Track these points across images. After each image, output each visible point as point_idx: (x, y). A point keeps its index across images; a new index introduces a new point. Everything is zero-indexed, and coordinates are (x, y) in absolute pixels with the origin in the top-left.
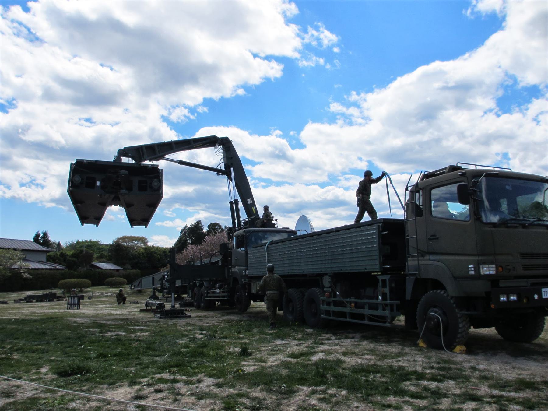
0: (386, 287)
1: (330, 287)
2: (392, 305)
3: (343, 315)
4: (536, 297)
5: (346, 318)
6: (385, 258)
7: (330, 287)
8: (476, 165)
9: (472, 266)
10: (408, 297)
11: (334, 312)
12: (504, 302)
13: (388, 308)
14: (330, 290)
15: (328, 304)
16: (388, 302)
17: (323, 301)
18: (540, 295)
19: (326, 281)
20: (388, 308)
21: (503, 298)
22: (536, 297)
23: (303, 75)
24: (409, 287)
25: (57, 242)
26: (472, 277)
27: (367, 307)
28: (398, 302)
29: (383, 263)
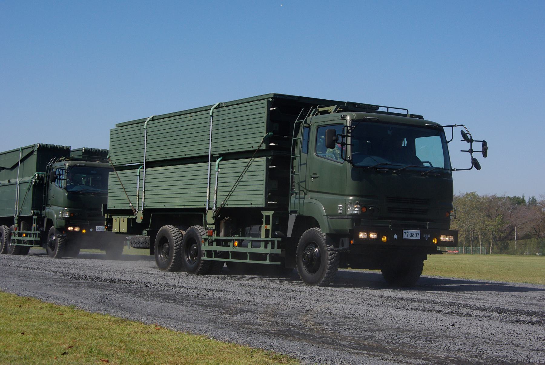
1: (213, 224)
2: (273, 242)
4: (396, 237)
5: (229, 258)
6: (270, 193)
7: (213, 224)
8: (388, 107)
9: (341, 205)
10: (289, 234)
12: (362, 239)
13: (269, 245)
14: (214, 227)
15: (211, 243)
17: (206, 240)
18: (400, 235)
19: (210, 217)
20: (269, 245)
22: (396, 237)
24: (292, 219)
27: (250, 245)
28: (280, 239)
29: (268, 199)
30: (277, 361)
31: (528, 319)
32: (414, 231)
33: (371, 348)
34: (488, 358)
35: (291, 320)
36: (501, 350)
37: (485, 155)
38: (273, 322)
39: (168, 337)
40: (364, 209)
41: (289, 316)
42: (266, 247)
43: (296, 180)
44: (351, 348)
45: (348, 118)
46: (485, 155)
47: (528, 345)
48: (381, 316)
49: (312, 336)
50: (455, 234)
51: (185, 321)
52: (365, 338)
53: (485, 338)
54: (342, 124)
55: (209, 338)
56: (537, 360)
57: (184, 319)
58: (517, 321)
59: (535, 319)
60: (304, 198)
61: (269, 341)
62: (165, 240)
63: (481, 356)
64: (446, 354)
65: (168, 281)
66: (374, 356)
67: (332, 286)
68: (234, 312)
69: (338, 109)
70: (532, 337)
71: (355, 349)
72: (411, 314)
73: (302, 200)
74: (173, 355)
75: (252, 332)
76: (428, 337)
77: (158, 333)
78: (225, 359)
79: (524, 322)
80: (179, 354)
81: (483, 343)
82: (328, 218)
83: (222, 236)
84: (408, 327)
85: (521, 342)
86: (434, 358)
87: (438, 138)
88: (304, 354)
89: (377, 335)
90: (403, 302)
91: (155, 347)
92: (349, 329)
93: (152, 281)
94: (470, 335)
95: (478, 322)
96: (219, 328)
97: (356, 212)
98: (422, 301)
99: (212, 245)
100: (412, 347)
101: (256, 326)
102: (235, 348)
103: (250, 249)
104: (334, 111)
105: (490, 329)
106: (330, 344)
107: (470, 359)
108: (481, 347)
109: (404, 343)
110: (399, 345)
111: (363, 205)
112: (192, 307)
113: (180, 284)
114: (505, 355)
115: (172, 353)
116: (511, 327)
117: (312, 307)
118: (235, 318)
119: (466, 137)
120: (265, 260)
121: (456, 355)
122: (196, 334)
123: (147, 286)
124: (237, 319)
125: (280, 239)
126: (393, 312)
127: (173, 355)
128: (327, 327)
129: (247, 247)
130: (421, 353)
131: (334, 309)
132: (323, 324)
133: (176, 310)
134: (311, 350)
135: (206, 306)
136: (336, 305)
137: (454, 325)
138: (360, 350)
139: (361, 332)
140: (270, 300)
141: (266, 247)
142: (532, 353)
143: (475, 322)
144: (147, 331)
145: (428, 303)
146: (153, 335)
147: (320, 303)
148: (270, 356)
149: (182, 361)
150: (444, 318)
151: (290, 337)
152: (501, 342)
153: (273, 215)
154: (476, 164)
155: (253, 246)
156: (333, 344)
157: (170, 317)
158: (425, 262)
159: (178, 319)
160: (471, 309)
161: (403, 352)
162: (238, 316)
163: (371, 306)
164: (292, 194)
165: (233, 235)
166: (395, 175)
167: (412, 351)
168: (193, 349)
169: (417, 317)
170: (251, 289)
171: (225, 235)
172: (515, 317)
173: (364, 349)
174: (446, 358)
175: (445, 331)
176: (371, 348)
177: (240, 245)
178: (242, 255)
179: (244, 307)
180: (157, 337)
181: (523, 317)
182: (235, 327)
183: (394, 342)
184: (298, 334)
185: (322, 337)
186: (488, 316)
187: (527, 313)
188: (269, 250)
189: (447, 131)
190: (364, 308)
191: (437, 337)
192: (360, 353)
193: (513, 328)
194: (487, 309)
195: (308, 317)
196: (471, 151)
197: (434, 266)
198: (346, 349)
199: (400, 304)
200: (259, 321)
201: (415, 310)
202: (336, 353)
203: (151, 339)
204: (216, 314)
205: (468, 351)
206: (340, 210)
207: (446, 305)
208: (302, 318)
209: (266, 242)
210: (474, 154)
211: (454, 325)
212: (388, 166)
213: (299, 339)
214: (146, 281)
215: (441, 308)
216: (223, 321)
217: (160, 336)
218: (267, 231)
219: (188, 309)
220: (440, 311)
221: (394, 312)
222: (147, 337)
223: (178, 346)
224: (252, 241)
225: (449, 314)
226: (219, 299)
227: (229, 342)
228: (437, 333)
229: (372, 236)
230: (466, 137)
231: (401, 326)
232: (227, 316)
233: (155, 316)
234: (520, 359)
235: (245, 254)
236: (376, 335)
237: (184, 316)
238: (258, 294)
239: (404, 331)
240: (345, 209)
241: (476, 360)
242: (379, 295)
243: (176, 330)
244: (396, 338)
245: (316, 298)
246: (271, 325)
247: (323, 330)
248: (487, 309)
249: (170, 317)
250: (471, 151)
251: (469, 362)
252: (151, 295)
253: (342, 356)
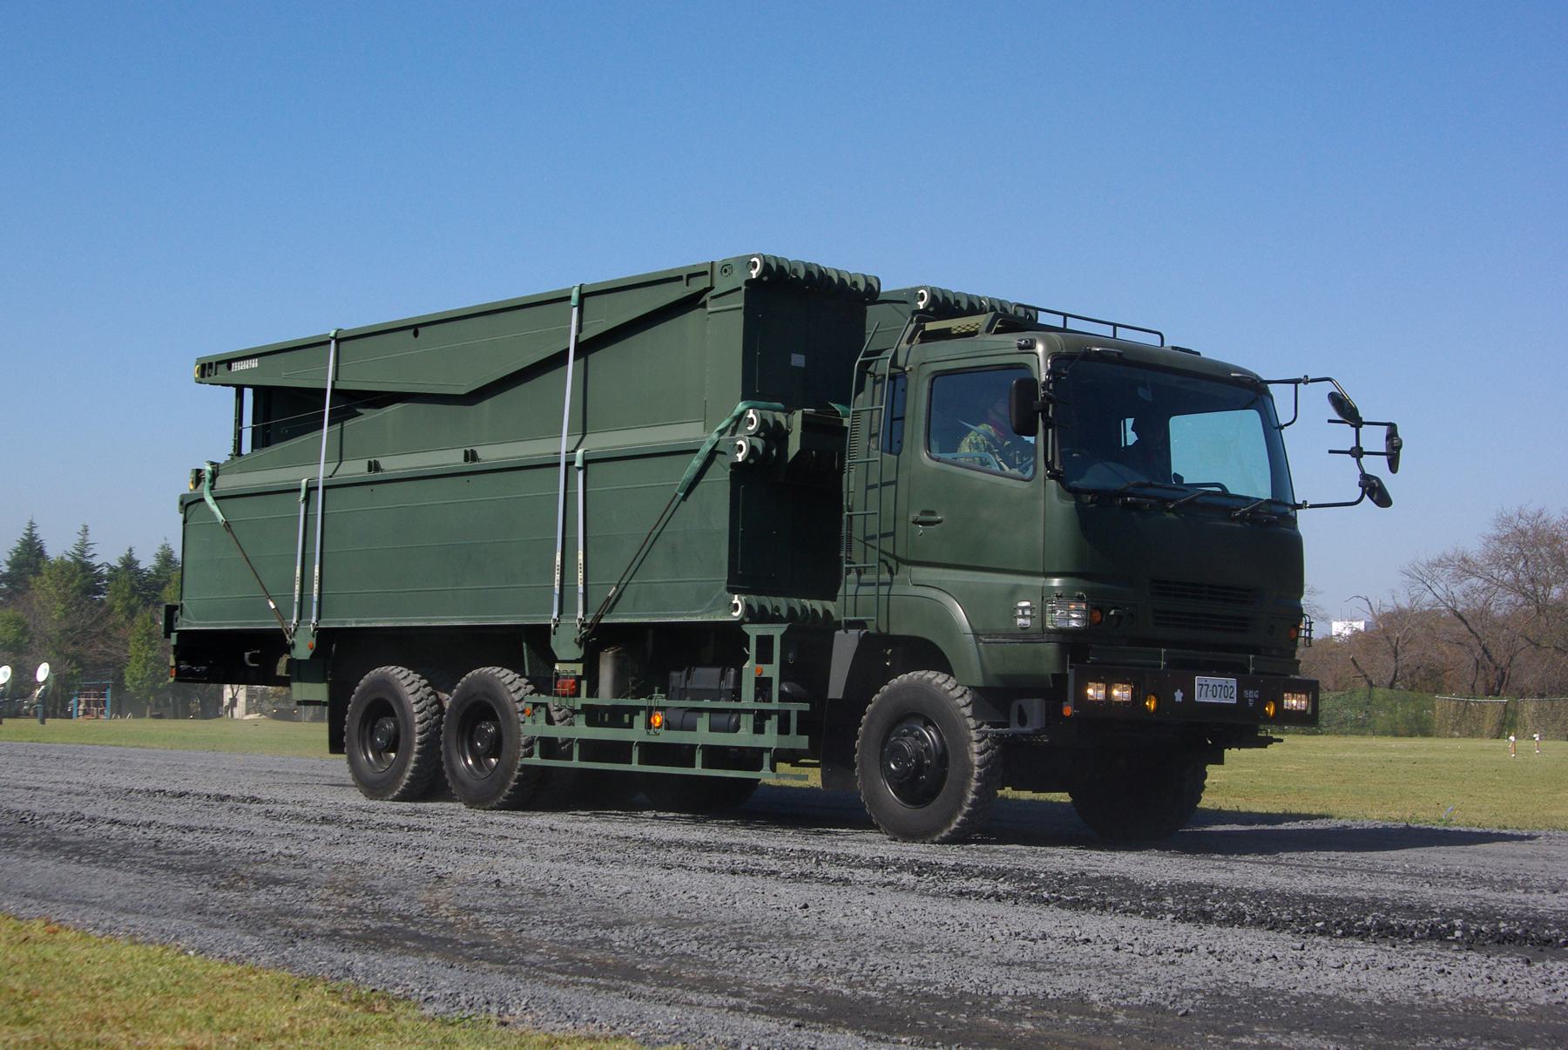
0: (769, 661)
1: (577, 661)
3: (620, 751)
4: (1179, 696)
10: (836, 689)
11: (584, 743)
13: (771, 725)
14: (579, 669)
16: (775, 704)
20: (771, 725)
21: (1094, 692)
22: (1179, 696)
23: (798, 360)
24: (845, 647)
25: (212, 425)
26: (1025, 635)
27: (703, 722)
28: (806, 707)
30: (361, 1007)
31: (987, 886)
32: (1222, 680)
33: (601, 969)
34: (890, 986)
35: (397, 903)
36: (922, 967)
37: (1393, 465)
38: (351, 908)
39: (79, 951)
40: (1097, 616)
41: (393, 892)
42: (759, 729)
43: (857, 533)
44: (549, 970)
45: (1040, 348)
46: (1393, 465)
47: (986, 952)
48: (625, 889)
49: (451, 941)
50: (1310, 688)
51: (124, 910)
52: (585, 945)
53: (882, 937)
54: (1023, 367)
55: (185, 952)
56: (1008, 987)
57: (121, 904)
58: (961, 894)
59: (1003, 887)
60: (890, 584)
61: (341, 958)
62: (383, 707)
63: (873, 983)
64: (786, 979)
65: (77, 808)
66: (609, 988)
67: (978, 842)
68: (251, 886)
69: (997, 325)
70: (996, 932)
71: (562, 972)
72: (701, 884)
73: (884, 590)
74: (93, 999)
75: (296, 933)
76: (743, 937)
77: (52, 943)
78: (228, 1006)
79: (979, 895)
80: (108, 995)
81: (878, 949)
82: (977, 640)
83: (605, 696)
84: (694, 915)
85: (971, 945)
86: (756, 989)
87: (1251, 417)
88: (430, 989)
89: (615, 935)
90: (681, 851)
91: (45, 977)
92: (545, 923)
93: (35, 806)
94: (846, 932)
95: (867, 898)
96: (212, 926)
97: (1074, 624)
98: (727, 848)
100: (704, 964)
101: (308, 921)
102: (254, 978)
103: (702, 735)
104: (988, 330)
105: (896, 916)
106: (496, 961)
107: (846, 992)
108: (873, 959)
109: (684, 954)
110: (671, 961)
111: (1096, 606)
112: (142, 873)
113: (110, 816)
114: (931, 977)
115: (89, 993)
116: (946, 907)
117: (450, 869)
118: (253, 899)
119: (1346, 411)
120: (758, 768)
121: (812, 981)
122: (152, 943)
123: (23, 821)
124: (258, 902)
125: (806, 707)
126: (656, 878)
127: (93, 999)
128: (489, 918)
129: (694, 729)
130: (725, 978)
131: (507, 873)
132: (479, 910)
133: (102, 881)
134: (447, 979)
135: (177, 871)
136: (511, 862)
137: (806, 906)
138: (572, 974)
139: (575, 929)
140: (343, 853)
141: (759, 729)
142: (996, 971)
143: (857, 897)
144: (23, 936)
145: (742, 852)
146: (39, 948)
147: (472, 857)
148: (345, 997)
149: (116, 1012)
150: (782, 890)
151: (395, 945)
152: (923, 945)
153: (783, 637)
154: (1375, 491)
156: (504, 962)
157: (82, 901)
158: (1211, 770)
159: (106, 906)
160: (849, 866)
161: (680, 976)
162: (262, 895)
163: (600, 862)
164: (849, 571)
165: (648, 693)
166: (1171, 516)
167: (703, 973)
168: (143, 982)
169: (715, 890)
170: (295, 826)
171: (618, 692)
172: (956, 884)
173: (584, 972)
174: (789, 989)
175: (785, 923)
176: (601, 969)
178: (682, 754)
179: (278, 872)
180: (50, 952)
181: (974, 884)
182: (254, 922)
183: (658, 952)
184: (416, 937)
185: (476, 945)
186: (890, 883)
187: (985, 873)
188: (770, 738)
189: (1281, 398)
190: (585, 869)
191: (765, 939)
192: (575, 984)
193: (952, 912)
194: (889, 864)
195: (441, 894)
196: (1357, 452)
197: (1235, 781)
198: (537, 972)
199: (674, 856)
200: (315, 907)
201: (709, 870)
202: (512, 984)
203: (35, 957)
204: (203, 891)
205: (841, 972)
206: (1024, 616)
207: (788, 857)
208: (426, 895)
209: (760, 719)
210: (1365, 460)
211: (806, 906)
212: (1150, 491)
213: (419, 952)
214: (20, 807)
215: (775, 865)
216: (222, 909)
217: (57, 949)
218: (763, 686)
219: (132, 877)
220: (773, 872)
221: (658, 876)
222: (23, 953)
223: (106, 975)
224: (712, 711)
225: (794, 878)
226: (213, 851)
227: (239, 961)
228: (765, 928)
229: (1120, 693)
230: (1346, 411)
231: (675, 914)
232: (232, 894)
233: (44, 897)
234: (967, 987)
235: (692, 748)
236: (613, 937)
237: (120, 896)
238: (311, 837)
239: (682, 924)
241: (861, 992)
242: (621, 834)
243: (99, 933)
244: (663, 943)
245: (461, 845)
246: (345, 916)
247: (478, 926)
248: (889, 864)
249: (82, 901)
250: (1357, 452)
251: (845, 998)
252: (34, 844)
253: (526, 991)
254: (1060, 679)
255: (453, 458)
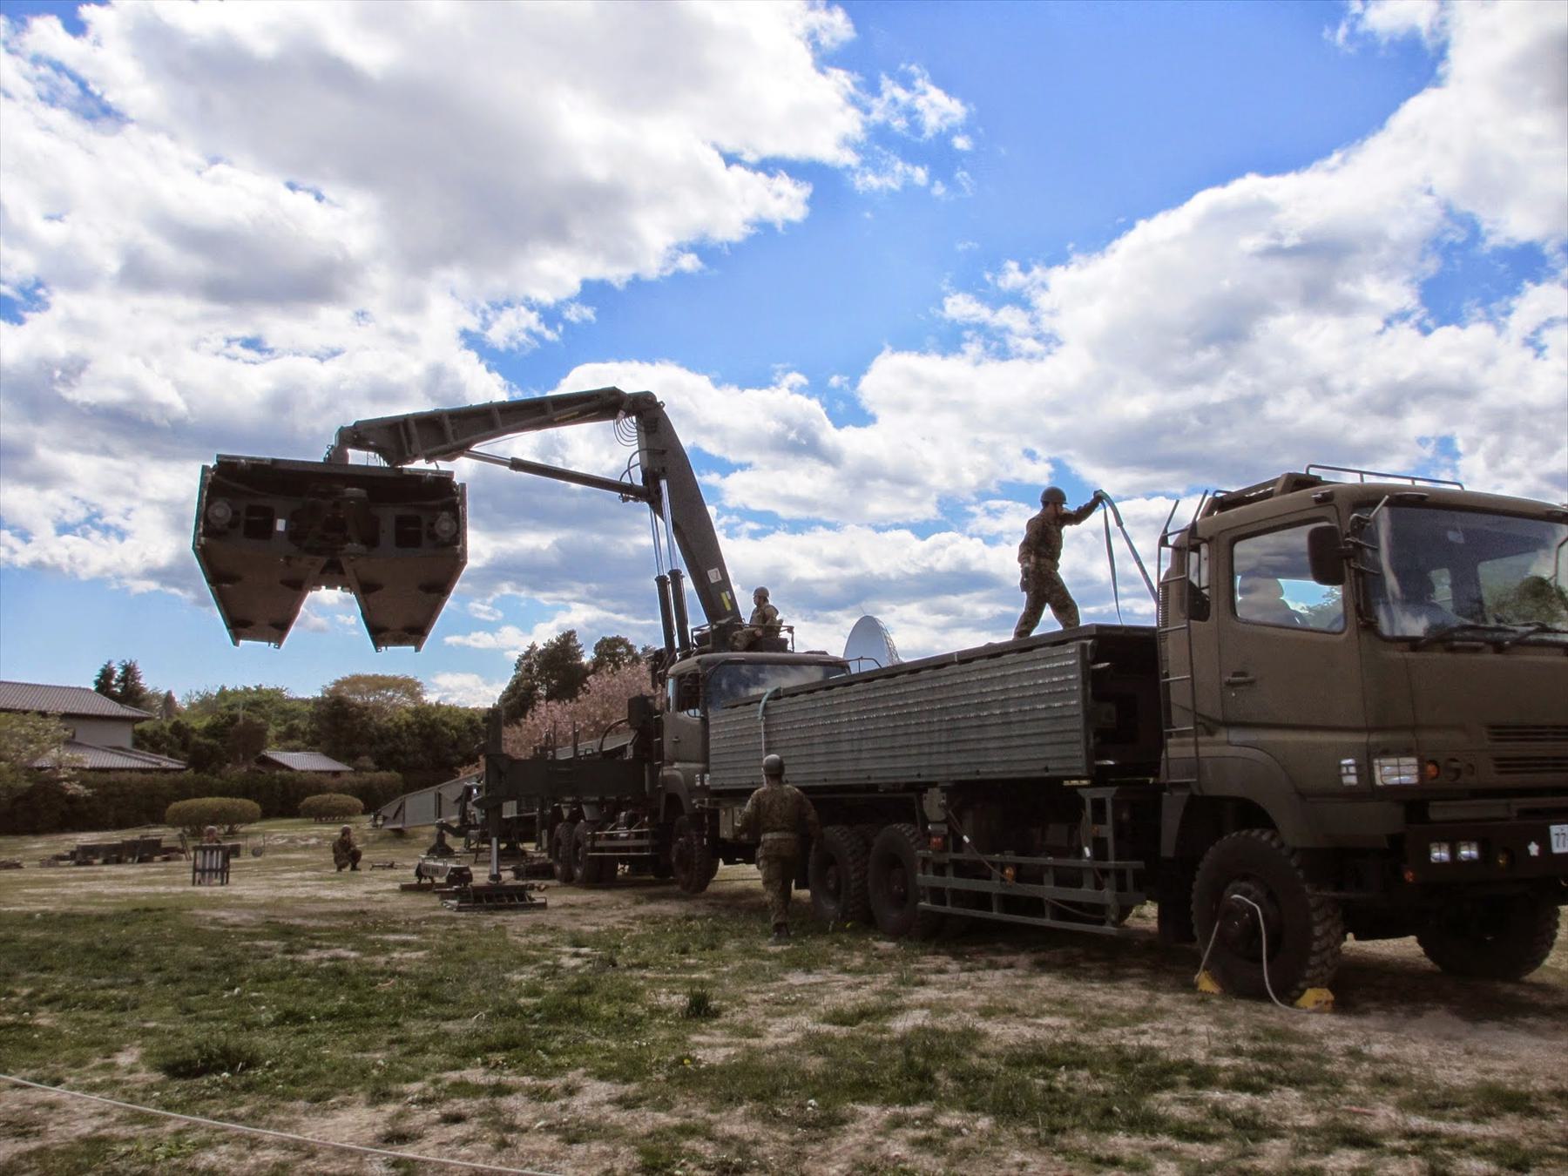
0: (1104, 822)
2: (1121, 874)
3: (983, 900)
4: (1534, 849)
5: (991, 910)
6: (1103, 738)
9: (1350, 761)
10: (1168, 848)
11: (955, 892)
12: (1441, 865)
15: (940, 870)
17: (925, 860)
18: (1545, 843)
19: (934, 804)
20: (1111, 881)
21: (1440, 854)
22: (1534, 849)
26: (1351, 794)
27: (1049, 877)
29: (1096, 753)
97: (1405, 779)
99: (943, 874)
155: (1059, 882)
177: (1019, 878)
229: (1468, 852)
240: (1365, 771)
254: (1396, 841)
255: (1418, 483)
